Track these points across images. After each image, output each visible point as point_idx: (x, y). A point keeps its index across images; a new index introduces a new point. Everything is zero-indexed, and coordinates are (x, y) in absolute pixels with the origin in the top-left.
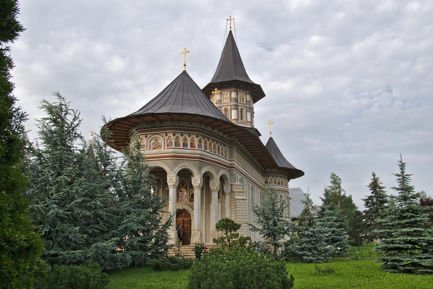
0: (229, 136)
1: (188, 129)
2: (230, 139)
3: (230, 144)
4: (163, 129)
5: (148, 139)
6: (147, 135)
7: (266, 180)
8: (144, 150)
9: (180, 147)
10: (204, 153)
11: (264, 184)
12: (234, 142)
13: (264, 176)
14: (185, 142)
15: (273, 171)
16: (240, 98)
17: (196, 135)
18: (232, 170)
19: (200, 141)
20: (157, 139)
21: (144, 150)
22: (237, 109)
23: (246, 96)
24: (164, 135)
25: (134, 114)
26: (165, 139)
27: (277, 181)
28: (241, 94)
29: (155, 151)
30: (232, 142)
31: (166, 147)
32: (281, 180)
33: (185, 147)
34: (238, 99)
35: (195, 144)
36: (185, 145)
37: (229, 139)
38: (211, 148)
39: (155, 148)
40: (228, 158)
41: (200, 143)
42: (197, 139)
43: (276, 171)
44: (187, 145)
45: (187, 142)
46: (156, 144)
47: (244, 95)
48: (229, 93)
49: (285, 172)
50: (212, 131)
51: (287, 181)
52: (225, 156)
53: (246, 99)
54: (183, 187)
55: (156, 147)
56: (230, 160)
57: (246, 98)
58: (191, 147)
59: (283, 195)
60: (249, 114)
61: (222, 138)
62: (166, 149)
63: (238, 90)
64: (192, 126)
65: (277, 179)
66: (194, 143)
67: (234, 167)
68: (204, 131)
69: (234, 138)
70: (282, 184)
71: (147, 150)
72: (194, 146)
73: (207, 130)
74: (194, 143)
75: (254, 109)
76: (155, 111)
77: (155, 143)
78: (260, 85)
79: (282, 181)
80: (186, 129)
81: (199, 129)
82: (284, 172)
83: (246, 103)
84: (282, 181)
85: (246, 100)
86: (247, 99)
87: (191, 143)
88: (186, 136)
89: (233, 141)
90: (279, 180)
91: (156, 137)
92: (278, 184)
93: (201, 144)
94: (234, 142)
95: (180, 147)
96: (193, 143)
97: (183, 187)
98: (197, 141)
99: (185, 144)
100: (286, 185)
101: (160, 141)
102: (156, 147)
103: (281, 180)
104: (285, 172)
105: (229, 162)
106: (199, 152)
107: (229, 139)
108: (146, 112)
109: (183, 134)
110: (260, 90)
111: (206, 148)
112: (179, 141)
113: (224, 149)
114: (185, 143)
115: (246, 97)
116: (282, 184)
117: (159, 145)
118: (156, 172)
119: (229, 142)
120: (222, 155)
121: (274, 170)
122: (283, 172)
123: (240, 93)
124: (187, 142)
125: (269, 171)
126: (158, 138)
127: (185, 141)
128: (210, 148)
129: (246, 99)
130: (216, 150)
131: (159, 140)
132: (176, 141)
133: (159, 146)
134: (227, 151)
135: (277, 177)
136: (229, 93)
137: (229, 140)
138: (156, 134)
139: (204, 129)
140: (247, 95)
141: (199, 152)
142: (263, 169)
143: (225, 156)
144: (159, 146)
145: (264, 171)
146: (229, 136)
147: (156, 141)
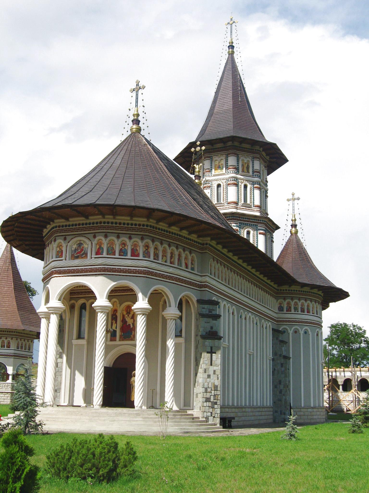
0: (199, 237)
1: (94, 226)
2: (200, 241)
3: (202, 249)
4: (90, 227)
5: (69, 242)
6: (67, 236)
7: (280, 304)
8: (62, 260)
9: (115, 255)
10: (153, 265)
11: (277, 311)
12: (208, 246)
13: (277, 298)
14: (123, 247)
15: (293, 289)
16: (243, 166)
17: (141, 236)
18: (204, 290)
19: (147, 247)
20: (81, 243)
21: (62, 260)
22: (237, 185)
23: (253, 162)
24: (90, 236)
25: (47, 206)
26: (92, 243)
27: (300, 306)
28: (245, 159)
29: (77, 262)
30: (205, 246)
31: (94, 256)
32: (306, 304)
33: (122, 256)
34: (238, 167)
35: (138, 250)
36: (123, 252)
37: (200, 240)
38: (166, 257)
39: (77, 257)
40: (198, 272)
41: (146, 250)
42: (142, 243)
43: (298, 289)
44: (126, 252)
45: (126, 248)
46: (79, 250)
47: (250, 160)
48: (223, 157)
49: (315, 291)
50: (169, 230)
51: (320, 307)
52: (193, 269)
53: (253, 168)
54: (128, 316)
55: (78, 254)
56: (201, 275)
57: (253, 166)
58: (132, 256)
59: (309, 330)
60: (257, 193)
61: (187, 240)
62: (93, 258)
63: (238, 152)
64: (134, 222)
65: (300, 304)
66: (137, 250)
67: (206, 286)
68: (154, 229)
69: (208, 240)
70: (308, 312)
71: (66, 260)
72: (136, 254)
73: (159, 229)
74: (138, 249)
75: (268, 184)
76: (75, 201)
77: (78, 249)
78: (275, 144)
79: (308, 306)
80: (125, 227)
81: (145, 227)
82: (312, 291)
83: (253, 174)
84: (308, 306)
85: (253, 170)
86: (255, 168)
87: (132, 250)
88: (125, 239)
89: (207, 244)
90: (302, 305)
91: (80, 241)
92: (307, 313)
93: (149, 250)
94: (208, 246)
95: (115, 255)
96: (135, 249)
97: (128, 316)
98: (141, 247)
99: (123, 251)
100: (315, 313)
101: (85, 246)
102: (78, 254)
103: (306, 304)
104: (316, 292)
105: (199, 278)
106: (144, 263)
107: (200, 240)
108: (59, 204)
109: (108, 234)
110: (279, 152)
111: (158, 257)
112: (114, 247)
113: (190, 258)
114: (123, 248)
115: (253, 164)
116: (308, 312)
117: (83, 252)
118: (82, 292)
119: (200, 245)
120: (187, 268)
121: (294, 288)
122: (311, 291)
123: (242, 158)
124: (126, 248)
125: (286, 290)
126: (82, 242)
127: (123, 246)
128: (165, 257)
129: (253, 168)
130: (174, 259)
131: (84, 245)
132: (109, 246)
133: (83, 254)
134: (196, 260)
135: (299, 300)
136: (223, 157)
137: (199, 243)
138: (80, 235)
139: (153, 227)
140: (255, 161)
141: (144, 263)
142: (276, 286)
143: (193, 269)
144: (83, 254)
145: (278, 290)
146: (199, 237)
147: (80, 246)
